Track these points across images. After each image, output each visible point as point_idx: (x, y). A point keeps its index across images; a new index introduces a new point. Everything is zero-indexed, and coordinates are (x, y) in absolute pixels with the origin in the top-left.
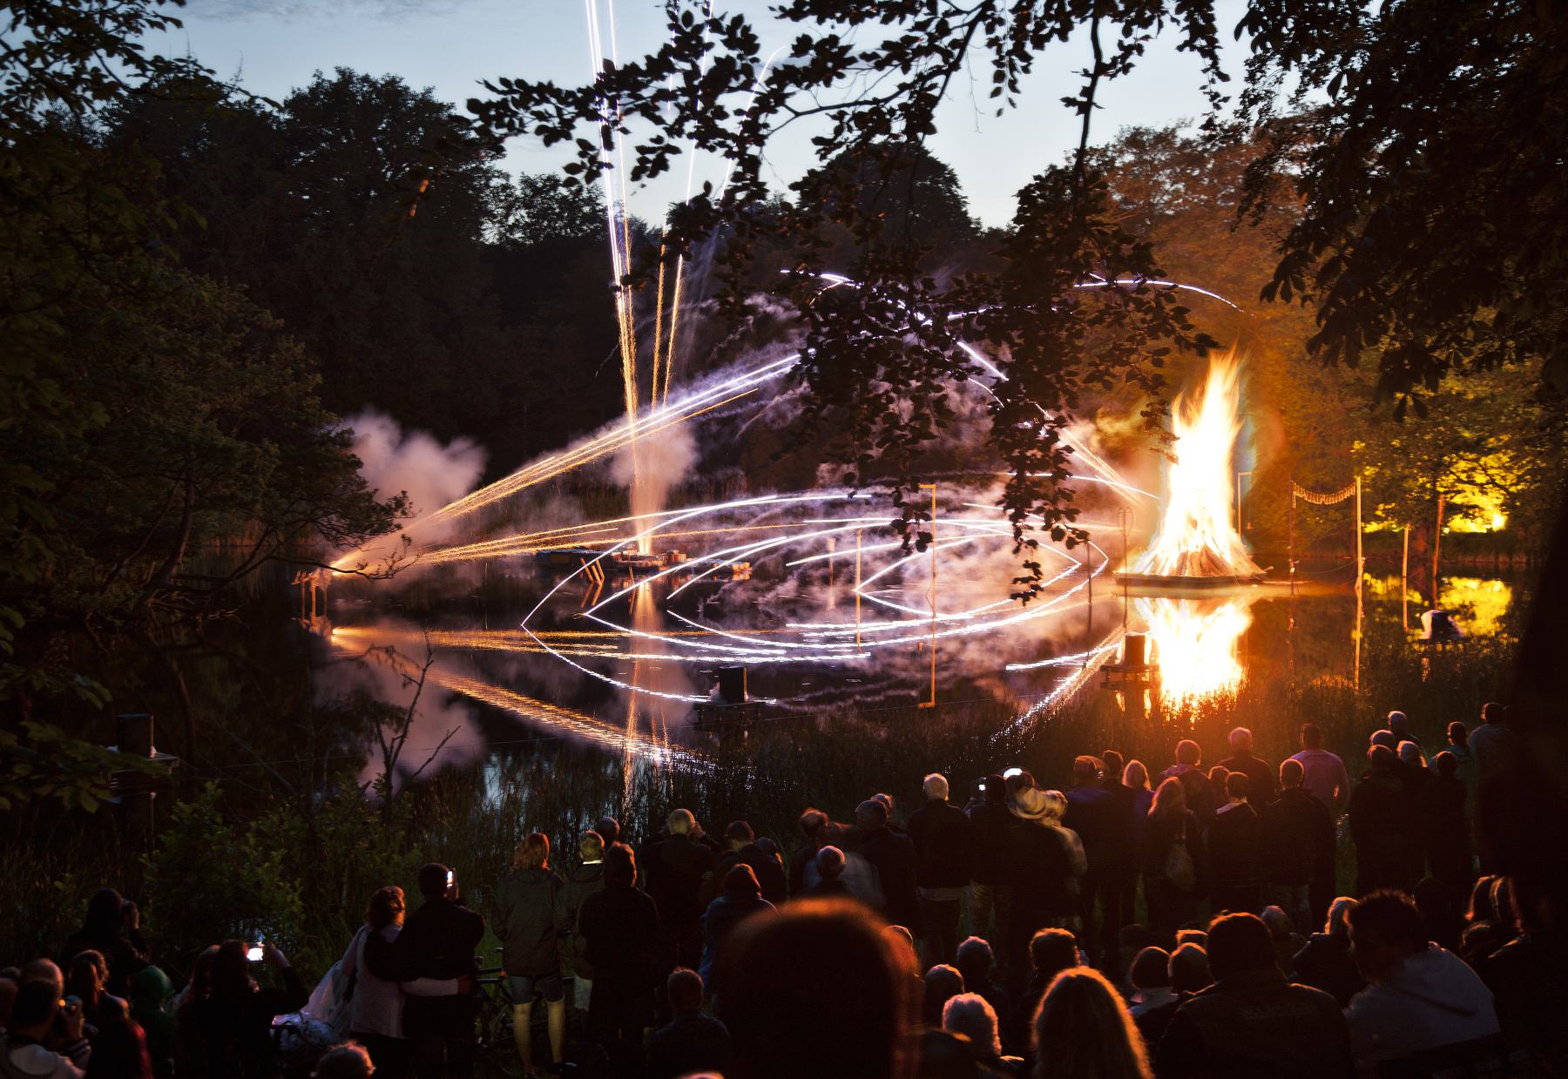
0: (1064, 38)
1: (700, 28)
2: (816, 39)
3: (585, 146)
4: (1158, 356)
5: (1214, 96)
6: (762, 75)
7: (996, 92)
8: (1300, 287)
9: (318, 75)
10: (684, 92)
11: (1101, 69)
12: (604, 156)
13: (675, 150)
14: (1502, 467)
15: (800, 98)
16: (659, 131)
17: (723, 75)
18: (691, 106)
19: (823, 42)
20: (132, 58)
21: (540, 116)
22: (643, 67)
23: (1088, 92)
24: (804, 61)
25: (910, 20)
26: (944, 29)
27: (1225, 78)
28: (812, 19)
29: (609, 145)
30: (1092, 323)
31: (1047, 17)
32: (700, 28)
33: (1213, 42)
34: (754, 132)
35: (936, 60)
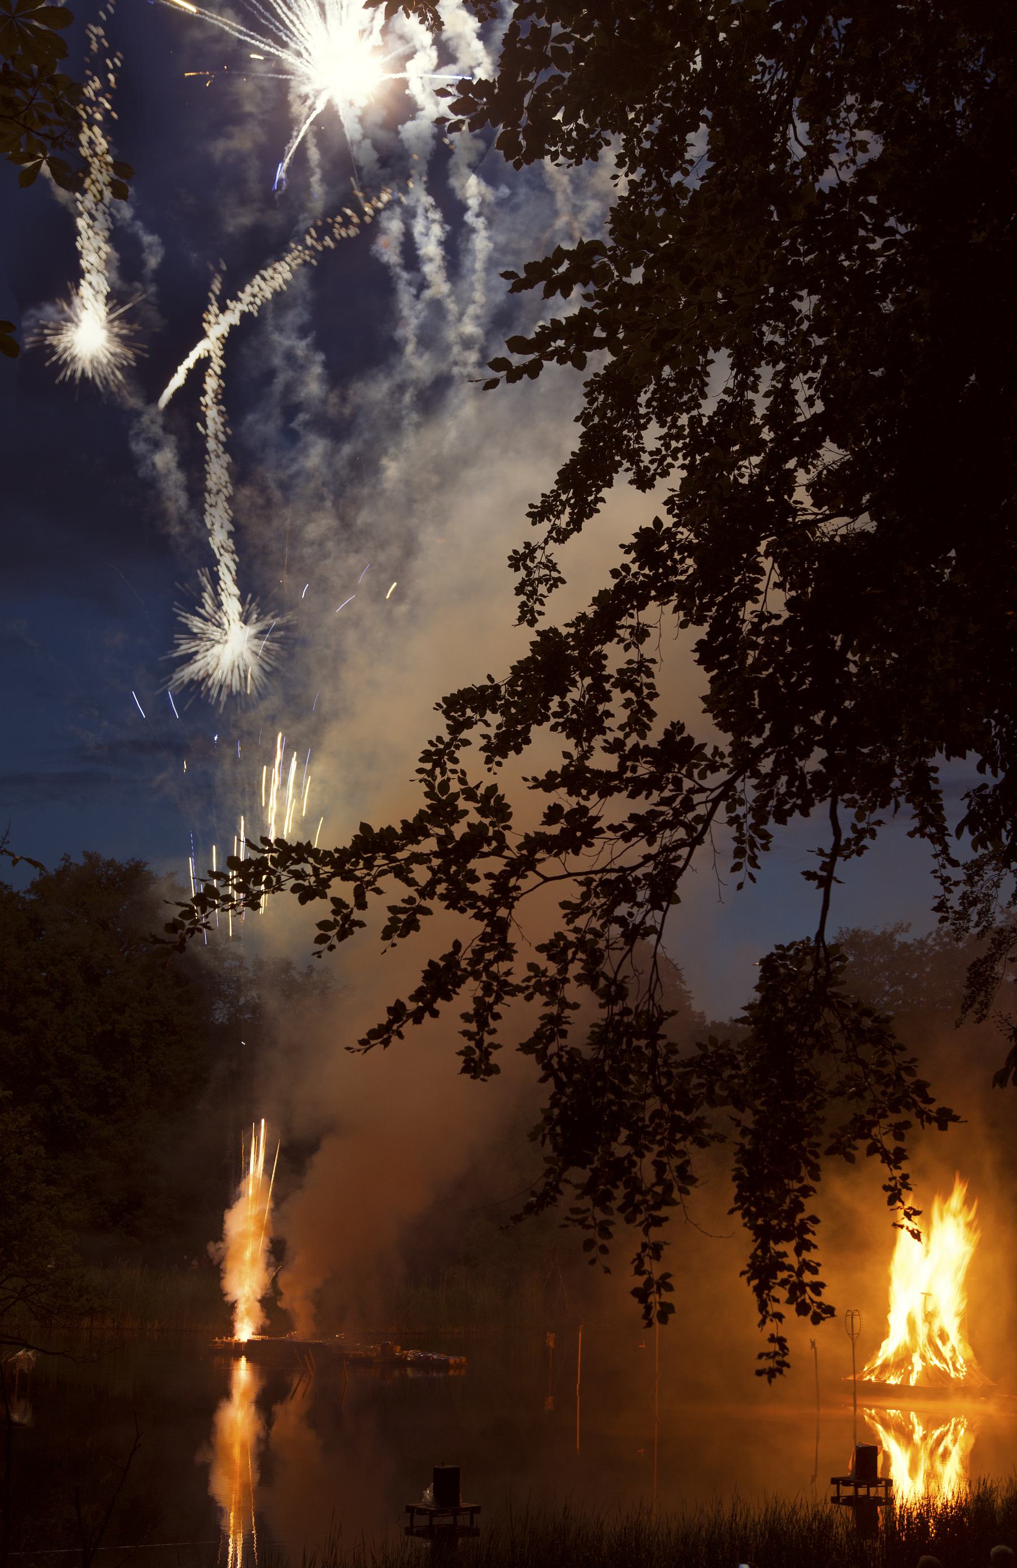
0: (805, 814)
1: (456, 796)
5: (945, 880)
7: (737, 867)
9: (66, 858)
10: (436, 855)
11: (837, 850)
12: (357, 915)
15: (550, 865)
16: (411, 892)
21: (298, 875)
22: (399, 829)
23: (828, 868)
24: (554, 830)
25: (656, 796)
26: (688, 805)
28: (563, 790)
29: (361, 904)
32: (456, 796)
33: (942, 830)
35: (681, 833)
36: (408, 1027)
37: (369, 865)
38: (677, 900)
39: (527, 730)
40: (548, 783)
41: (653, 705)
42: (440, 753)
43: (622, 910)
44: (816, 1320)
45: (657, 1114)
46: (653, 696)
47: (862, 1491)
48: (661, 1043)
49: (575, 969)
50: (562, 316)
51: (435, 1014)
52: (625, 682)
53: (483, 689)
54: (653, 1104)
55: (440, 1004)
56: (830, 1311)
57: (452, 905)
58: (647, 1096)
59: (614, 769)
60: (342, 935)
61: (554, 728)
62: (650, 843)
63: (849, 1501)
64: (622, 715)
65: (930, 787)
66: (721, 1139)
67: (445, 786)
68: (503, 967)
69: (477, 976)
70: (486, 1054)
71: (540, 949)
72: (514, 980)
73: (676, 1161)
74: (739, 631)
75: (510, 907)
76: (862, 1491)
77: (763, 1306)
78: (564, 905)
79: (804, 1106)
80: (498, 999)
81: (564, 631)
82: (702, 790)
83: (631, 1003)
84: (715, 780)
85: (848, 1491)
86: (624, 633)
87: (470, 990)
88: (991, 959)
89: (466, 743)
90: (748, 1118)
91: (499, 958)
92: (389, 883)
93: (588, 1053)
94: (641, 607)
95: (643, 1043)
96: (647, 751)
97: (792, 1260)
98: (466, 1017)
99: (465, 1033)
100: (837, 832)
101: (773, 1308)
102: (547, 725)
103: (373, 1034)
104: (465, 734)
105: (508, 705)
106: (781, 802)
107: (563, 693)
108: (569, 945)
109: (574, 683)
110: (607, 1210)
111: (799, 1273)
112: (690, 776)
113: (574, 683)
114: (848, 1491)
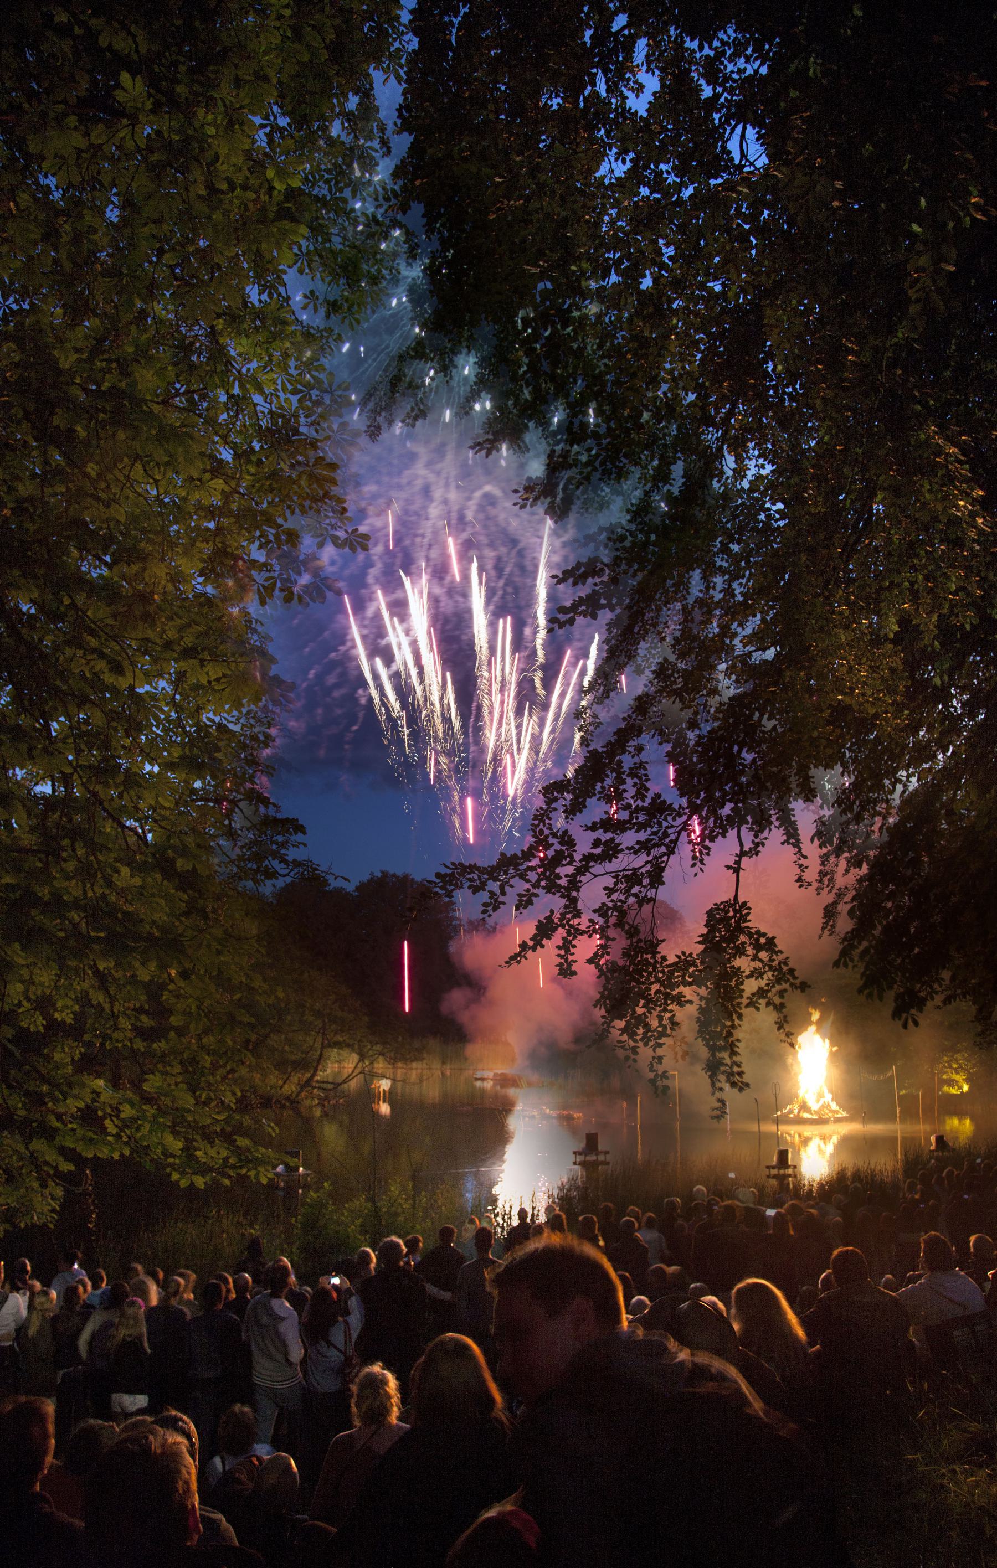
0: (724, 836)
1: (547, 837)
2: (603, 840)
3: (492, 894)
4: (781, 993)
5: (801, 866)
6: (577, 857)
7: (693, 865)
8: (852, 960)
9: (372, 874)
10: (539, 867)
11: (743, 854)
12: (501, 899)
13: (536, 895)
14: (965, 1059)
15: (597, 868)
16: (527, 886)
17: (557, 860)
18: (543, 873)
19: (607, 841)
20: (283, 860)
21: (471, 880)
22: (520, 855)
23: (738, 862)
24: (598, 851)
25: (649, 831)
26: (666, 835)
27: (805, 857)
28: (601, 831)
29: (503, 893)
30: (748, 977)
31: (715, 826)
32: (547, 837)
33: (798, 841)
34: (574, 884)
35: (663, 849)
36: (529, 954)
37: (506, 873)
38: (663, 883)
39: (584, 801)
40: (593, 827)
41: (648, 785)
42: (542, 815)
43: (636, 889)
44: (741, 1090)
45: (658, 991)
46: (647, 780)
47: (782, 1172)
48: (658, 956)
49: (612, 920)
50: (583, 595)
51: (543, 946)
52: (632, 774)
53: (562, 781)
54: (655, 987)
55: (545, 942)
56: (747, 1085)
57: (549, 891)
58: (652, 983)
59: (627, 818)
60: (495, 909)
61: (599, 799)
62: (648, 854)
63: (775, 1177)
64: (632, 791)
65: (916, 790)
66: (691, 1002)
67: (541, 832)
68: (575, 922)
69: (563, 927)
70: (570, 965)
71: (594, 911)
72: (582, 927)
73: (668, 1015)
74: (688, 745)
75: (578, 891)
76: (782, 1172)
77: (713, 1085)
78: (605, 889)
79: (733, 984)
80: (575, 938)
81: (600, 750)
82: (672, 826)
83: (642, 936)
84: (679, 821)
85: (774, 1172)
86: (631, 749)
87: (561, 932)
88: (835, 903)
89: (555, 809)
90: (703, 991)
91: (573, 917)
92: (516, 881)
93: (621, 963)
94: (639, 736)
95: (649, 956)
96: (643, 809)
97: (728, 1061)
98: (559, 948)
99: (559, 955)
100: (741, 845)
101: (718, 1085)
102: (594, 799)
103: (512, 958)
104: (554, 805)
105: (575, 789)
106: (712, 831)
107: (602, 781)
108: (609, 908)
109: (607, 776)
110: (636, 1041)
111: (731, 1067)
112: (666, 820)
113: (607, 776)
114: (774, 1172)
